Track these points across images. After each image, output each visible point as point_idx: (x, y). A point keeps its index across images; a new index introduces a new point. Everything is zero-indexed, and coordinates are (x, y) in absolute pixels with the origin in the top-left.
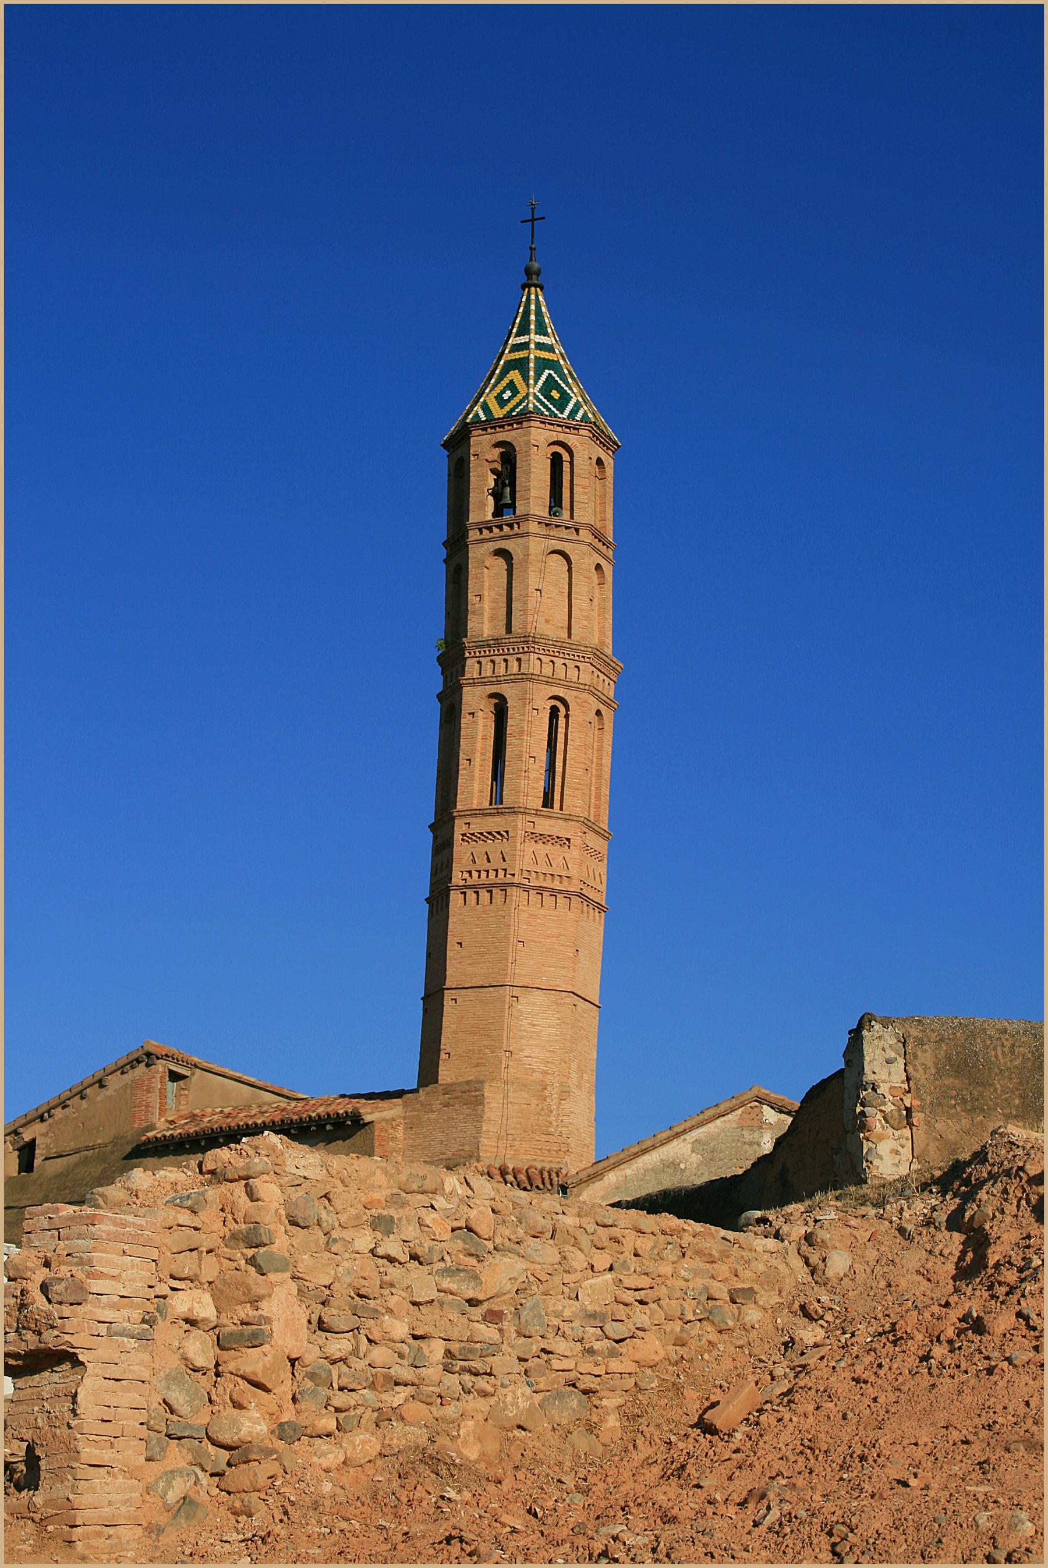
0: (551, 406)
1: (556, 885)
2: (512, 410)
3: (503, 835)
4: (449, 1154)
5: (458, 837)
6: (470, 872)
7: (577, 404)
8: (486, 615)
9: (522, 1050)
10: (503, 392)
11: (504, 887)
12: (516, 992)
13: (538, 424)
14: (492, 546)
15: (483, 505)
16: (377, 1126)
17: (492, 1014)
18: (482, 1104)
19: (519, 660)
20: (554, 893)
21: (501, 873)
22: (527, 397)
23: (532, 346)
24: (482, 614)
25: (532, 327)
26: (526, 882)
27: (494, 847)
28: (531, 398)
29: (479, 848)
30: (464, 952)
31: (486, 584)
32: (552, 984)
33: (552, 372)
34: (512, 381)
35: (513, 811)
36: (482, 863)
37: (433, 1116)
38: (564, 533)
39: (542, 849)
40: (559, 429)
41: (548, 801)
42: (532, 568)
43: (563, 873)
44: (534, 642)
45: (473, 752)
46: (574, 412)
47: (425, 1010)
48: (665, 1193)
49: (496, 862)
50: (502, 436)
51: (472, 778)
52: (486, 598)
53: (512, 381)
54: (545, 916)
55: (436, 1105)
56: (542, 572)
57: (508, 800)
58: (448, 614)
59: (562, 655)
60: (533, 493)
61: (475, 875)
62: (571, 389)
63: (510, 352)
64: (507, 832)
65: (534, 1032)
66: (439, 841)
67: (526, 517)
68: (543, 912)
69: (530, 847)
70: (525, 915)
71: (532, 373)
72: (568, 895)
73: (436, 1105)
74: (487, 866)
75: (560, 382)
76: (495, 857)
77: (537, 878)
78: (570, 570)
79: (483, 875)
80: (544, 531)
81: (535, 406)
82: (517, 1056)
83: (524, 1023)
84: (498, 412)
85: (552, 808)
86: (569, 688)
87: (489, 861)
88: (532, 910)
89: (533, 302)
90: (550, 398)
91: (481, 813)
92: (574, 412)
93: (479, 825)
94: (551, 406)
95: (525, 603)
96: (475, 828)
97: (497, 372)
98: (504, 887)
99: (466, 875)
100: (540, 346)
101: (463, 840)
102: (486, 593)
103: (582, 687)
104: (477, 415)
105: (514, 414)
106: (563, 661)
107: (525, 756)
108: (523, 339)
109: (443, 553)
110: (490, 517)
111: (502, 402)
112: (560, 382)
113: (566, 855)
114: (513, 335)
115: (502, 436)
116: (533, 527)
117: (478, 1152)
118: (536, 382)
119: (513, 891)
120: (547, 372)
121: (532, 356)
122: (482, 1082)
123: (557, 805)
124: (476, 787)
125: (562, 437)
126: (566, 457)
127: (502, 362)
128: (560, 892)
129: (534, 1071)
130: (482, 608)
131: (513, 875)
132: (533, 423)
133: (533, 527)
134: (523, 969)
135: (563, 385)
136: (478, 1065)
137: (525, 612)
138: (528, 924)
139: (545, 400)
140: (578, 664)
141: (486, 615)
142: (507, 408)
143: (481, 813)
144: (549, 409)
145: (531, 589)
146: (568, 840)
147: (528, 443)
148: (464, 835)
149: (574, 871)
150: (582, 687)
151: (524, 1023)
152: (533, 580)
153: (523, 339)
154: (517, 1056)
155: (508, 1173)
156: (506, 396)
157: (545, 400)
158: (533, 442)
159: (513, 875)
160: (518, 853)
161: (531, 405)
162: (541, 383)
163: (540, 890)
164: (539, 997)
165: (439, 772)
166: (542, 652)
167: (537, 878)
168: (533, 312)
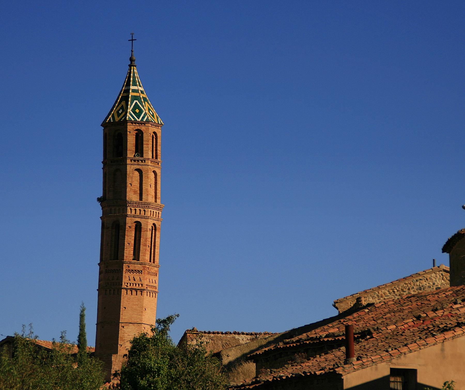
0: (135, 116)
7: (146, 114)
10: (119, 110)
11: (142, 291)
13: (130, 124)
21: (140, 285)
25: (131, 83)
27: (137, 276)
28: (128, 114)
32: (135, 321)
33: (137, 101)
43: (139, 283)
46: (143, 118)
48: (85, 340)
62: (143, 107)
71: (129, 103)
74: (133, 282)
75: (140, 105)
79: (137, 285)
81: (129, 117)
86: (141, 218)
87: (135, 280)
90: (135, 113)
92: (143, 118)
94: (135, 116)
96: (131, 268)
109: (102, 165)
111: (119, 115)
112: (140, 105)
119: (145, 293)
128: (139, 289)
135: (141, 106)
138: (127, 301)
139: (133, 114)
156: (120, 112)
157: (134, 115)
162: (131, 108)
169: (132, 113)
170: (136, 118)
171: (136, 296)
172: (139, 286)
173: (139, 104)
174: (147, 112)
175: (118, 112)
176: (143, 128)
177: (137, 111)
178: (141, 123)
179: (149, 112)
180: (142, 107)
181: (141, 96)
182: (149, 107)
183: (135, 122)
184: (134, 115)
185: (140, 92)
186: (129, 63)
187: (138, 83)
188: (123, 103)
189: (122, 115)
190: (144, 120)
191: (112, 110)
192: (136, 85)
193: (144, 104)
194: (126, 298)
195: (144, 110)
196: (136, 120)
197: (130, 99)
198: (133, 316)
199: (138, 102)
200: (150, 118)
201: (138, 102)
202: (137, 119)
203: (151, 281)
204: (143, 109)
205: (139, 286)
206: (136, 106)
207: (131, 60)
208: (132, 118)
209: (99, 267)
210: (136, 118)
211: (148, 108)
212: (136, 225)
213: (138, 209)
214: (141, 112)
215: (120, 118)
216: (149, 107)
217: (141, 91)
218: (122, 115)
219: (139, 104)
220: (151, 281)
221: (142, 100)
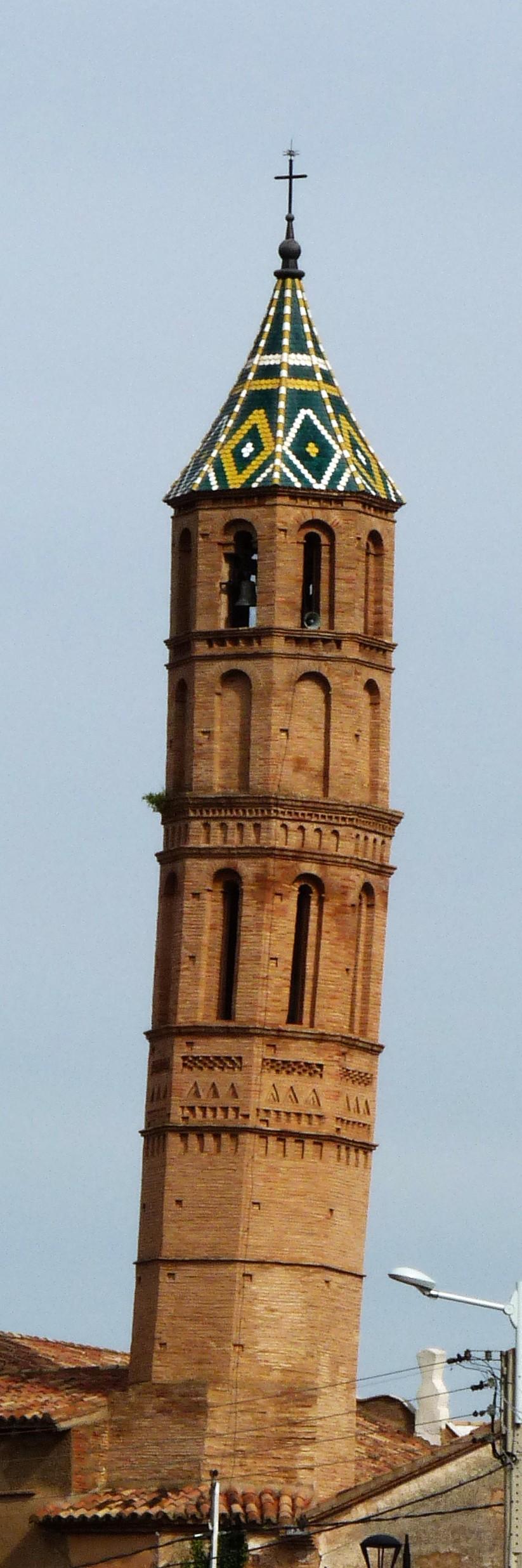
0: (305, 472)
1: (304, 1127)
2: (253, 478)
3: (234, 1063)
4: (164, 1472)
5: (177, 1060)
6: (192, 1109)
7: (343, 464)
8: (217, 759)
9: (256, 1343)
10: (242, 444)
12: (249, 1269)
14: (223, 667)
15: (213, 608)
16: (73, 1435)
17: (219, 1297)
18: (205, 1413)
19: (257, 827)
20: (300, 1138)
22: (271, 458)
23: (284, 373)
24: (211, 759)
25: (286, 342)
26: (264, 1126)
27: (223, 1078)
29: (204, 1078)
30: (185, 1213)
31: (218, 716)
32: (296, 1257)
33: (309, 412)
34: (240, 472)
35: (244, 1033)
36: (205, 1098)
37: (145, 1423)
38: (320, 650)
39: (286, 1081)
40: (315, 504)
41: (294, 1015)
42: (275, 700)
43: (313, 1111)
44: (277, 805)
45: (198, 946)
46: (337, 477)
47: (139, 1280)
49: (225, 1099)
50: (238, 513)
51: (196, 981)
52: (217, 736)
53: (240, 472)
54: (288, 1169)
55: (149, 1410)
56: (289, 707)
57: (242, 1014)
58: (170, 743)
59: (314, 819)
60: (279, 597)
61: (198, 1112)
63: (255, 378)
64: (240, 1059)
65: (273, 1320)
66: (158, 1057)
67: (264, 632)
68: (287, 1163)
69: (269, 1079)
70: (262, 1169)
72: (319, 1140)
73: (149, 1410)
74: (213, 1102)
76: (223, 1090)
77: (278, 1119)
78: (327, 701)
79: (209, 1114)
80: (292, 649)
81: (283, 474)
82: (250, 1351)
83: (259, 1307)
84: (235, 481)
85: (301, 1023)
88: (272, 1161)
89: (288, 301)
90: (303, 457)
91: (207, 1032)
92: (337, 477)
93: (203, 1048)
94: (305, 472)
95: (267, 748)
97: (237, 409)
98: (235, 1133)
99: (187, 1112)
100: (298, 372)
101: (184, 1065)
102: (217, 729)
103: (341, 860)
104: (206, 480)
105: (255, 485)
106: (315, 826)
107: (265, 959)
108: (271, 360)
109: (165, 654)
110: (222, 626)
111: (241, 463)
112: (321, 427)
113: (317, 1087)
114: (260, 351)
115: (238, 513)
116: (278, 645)
117: (199, 1474)
118: (284, 440)
120: (303, 413)
121: (283, 391)
122: (204, 1385)
123: (306, 1019)
124: (202, 993)
125: (319, 515)
126: (324, 540)
127: (244, 394)
128: (308, 1136)
129: (271, 1369)
130: (211, 751)
131: (247, 1116)
132: (279, 500)
133: (278, 645)
134: (259, 1237)
135: (324, 432)
136: (200, 1363)
137: (266, 761)
138: (267, 1180)
139: (297, 462)
140: (337, 828)
141: (217, 759)
142: (246, 474)
143: (207, 1032)
144: (301, 477)
145: (275, 729)
146: (320, 1066)
147: (272, 526)
148: (184, 1058)
149: (328, 1107)
150: (341, 860)
151: (259, 1307)
152: (278, 717)
153: (271, 360)
154: (250, 1351)
155: (235, 1502)
157: (300, 466)
158: (280, 525)
159: (247, 1116)
160: (254, 1087)
161: (277, 475)
163: (282, 1136)
164: (280, 1275)
165: (157, 960)
166: (286, 817)
167: (278, 1119)
168: (287, 318)
169: (293, 458)
170: (308, 476)
171: (302, 1163)
172: (204, 1115)
173: (317, 422)
174: (347, 454)
175: (237, 453)
176: (334, 517)
177: (312, 450)
178: (331, 498)
179: (367, 460)
180: (328, 437)
181: (324, 395)
182: (354, 434)
183: (307, 494)
184: (300, 466)
185: (319, 376)
186: (278, 263)
187: (310, 344)
188: (258, 417)
189: (255, 465)
190: (340, 488)
191: (210, 442)
192: (304, 350)
193: (334, 424)
194: (262, 1169)
195: (336, 447)
196: (310, 488)
197: (282, 405)
198: (289, 1236)
199: (313, 417)
200: (359, 480)
201: (313, 417)
202: (312, 481)
203: (353, 1105)
204: (332, 442)
205: (204, 1115)
206: (308, 433)
207: (289, 253)
208: (294, 479)
209: (147, 1044)
210: (308, 476)
211: (352, 439)
212: (300, 889)
213: (310, 828)
214: (326, 453)
215: (246, 474)
216: (354, 434)
217: (323, 372)
218: (255, 465)
219: (317, 422)
220: (353, 1105)
221: (330, 409)
